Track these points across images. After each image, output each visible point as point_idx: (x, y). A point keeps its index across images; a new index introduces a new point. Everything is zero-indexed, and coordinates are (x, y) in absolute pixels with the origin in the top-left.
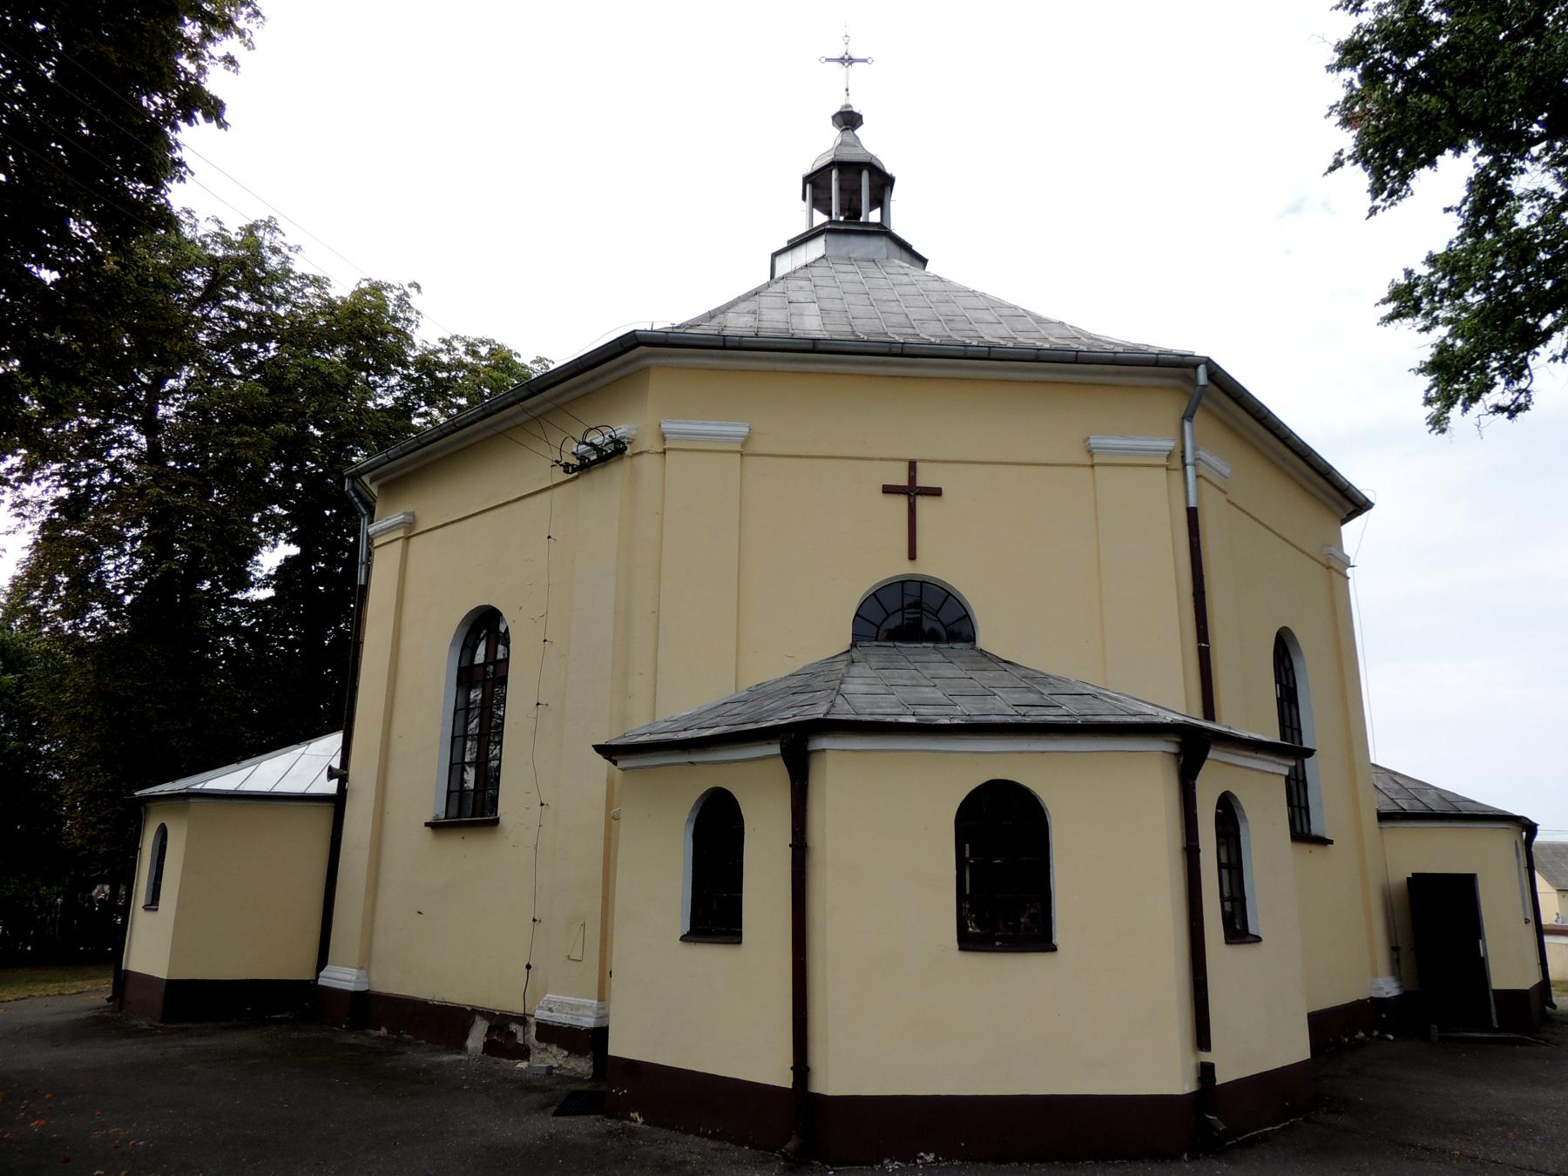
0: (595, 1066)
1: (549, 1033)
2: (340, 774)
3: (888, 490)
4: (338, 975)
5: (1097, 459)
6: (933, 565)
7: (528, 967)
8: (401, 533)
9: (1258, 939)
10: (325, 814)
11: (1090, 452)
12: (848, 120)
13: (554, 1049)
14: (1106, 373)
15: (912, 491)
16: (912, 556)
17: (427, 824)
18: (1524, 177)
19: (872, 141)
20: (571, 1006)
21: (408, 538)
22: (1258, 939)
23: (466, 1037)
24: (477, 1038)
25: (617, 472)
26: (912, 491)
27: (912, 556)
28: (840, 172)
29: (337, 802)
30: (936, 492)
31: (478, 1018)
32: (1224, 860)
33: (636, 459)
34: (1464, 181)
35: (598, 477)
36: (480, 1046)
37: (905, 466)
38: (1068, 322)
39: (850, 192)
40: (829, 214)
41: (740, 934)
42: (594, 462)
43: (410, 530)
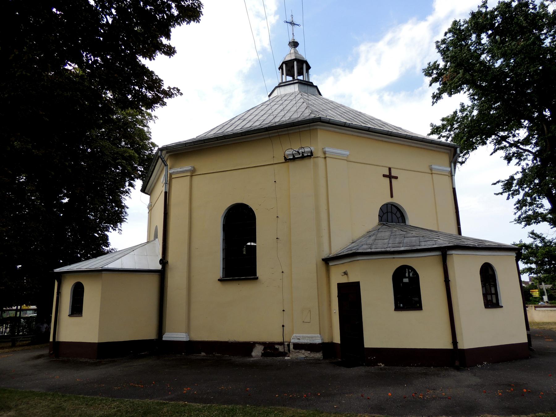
0: (323, 355)
1: (298, 346)
2: (164, 262)
3: (384, 176)
4: (180, 336)
5: (433, 172)
6: (395, 200)
7: (283, 326)
8: (189, 174)
9: (502, 307)
10: (154, 280)
11: (431, 169)
12: (295, 44)
13: (303, 351)
14: (434, 147)
15: (390, 177)
16: (392, 196)
17: (219, 280)
18: (393, 74)
19: (303, 52)
20: (309, 337)
21: (192, 176)
22: (502, 307)
23: (252, 351)
24: (257, 352)
25: (309, 163)
26: (390, 177)
27: (392, 196)
28: (297, 63)
29: (162, 274)
30: (396, 178)
31: (257, 345)
32: (10, 344)
33: (315, 159)
34: (359, 69)
35: (291, 165)
36: (260, 354)
37: (388, 169)
38: (403, 128)
39: (296, 68)
40: (293, 76)
41: (420, 302)
42: (290, 159)
43: (193, 173)
